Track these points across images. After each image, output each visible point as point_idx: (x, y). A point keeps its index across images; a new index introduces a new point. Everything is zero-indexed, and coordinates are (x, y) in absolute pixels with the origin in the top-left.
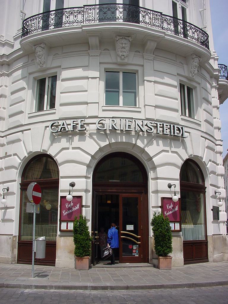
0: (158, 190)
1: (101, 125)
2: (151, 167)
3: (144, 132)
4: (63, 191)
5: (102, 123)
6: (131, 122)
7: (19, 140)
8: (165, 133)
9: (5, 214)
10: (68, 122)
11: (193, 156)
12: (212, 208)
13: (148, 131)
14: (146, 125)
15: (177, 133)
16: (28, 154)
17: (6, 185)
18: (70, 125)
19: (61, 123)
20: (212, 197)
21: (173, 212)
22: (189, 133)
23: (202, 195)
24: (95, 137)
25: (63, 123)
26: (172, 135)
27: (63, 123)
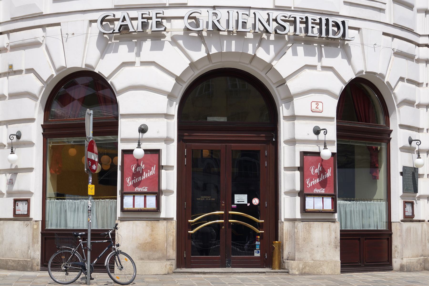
0: (294, 138)
1: (194, 20)
2: (283, 96)
3: (270, 33)
4: (126, 140)
5: (195, 17)
6: (247, 15)
7: (36, 44)
8: (310, 34)
9: (11, 182)
10: (133, 14)
11: (364, 73)
12: (402, 171)
13: (278, 31)
14: (275, 20)
15: (334, 33)
16: (57, 71)
17: (14, 129)
18: (136, 19)
19: (119, 14)
20: (403, 149)
21: (321, 179)
22: (358, 29)
23: (384, 146)
24: (181, 42)
25: (124, 16)
26: (323, 37)
27: (124, 17)
